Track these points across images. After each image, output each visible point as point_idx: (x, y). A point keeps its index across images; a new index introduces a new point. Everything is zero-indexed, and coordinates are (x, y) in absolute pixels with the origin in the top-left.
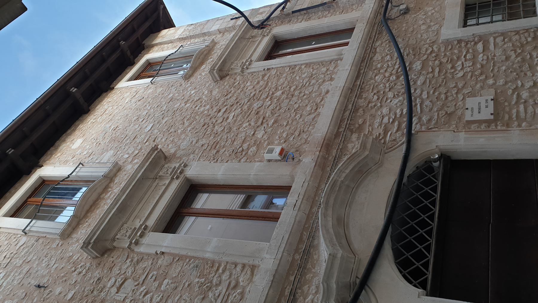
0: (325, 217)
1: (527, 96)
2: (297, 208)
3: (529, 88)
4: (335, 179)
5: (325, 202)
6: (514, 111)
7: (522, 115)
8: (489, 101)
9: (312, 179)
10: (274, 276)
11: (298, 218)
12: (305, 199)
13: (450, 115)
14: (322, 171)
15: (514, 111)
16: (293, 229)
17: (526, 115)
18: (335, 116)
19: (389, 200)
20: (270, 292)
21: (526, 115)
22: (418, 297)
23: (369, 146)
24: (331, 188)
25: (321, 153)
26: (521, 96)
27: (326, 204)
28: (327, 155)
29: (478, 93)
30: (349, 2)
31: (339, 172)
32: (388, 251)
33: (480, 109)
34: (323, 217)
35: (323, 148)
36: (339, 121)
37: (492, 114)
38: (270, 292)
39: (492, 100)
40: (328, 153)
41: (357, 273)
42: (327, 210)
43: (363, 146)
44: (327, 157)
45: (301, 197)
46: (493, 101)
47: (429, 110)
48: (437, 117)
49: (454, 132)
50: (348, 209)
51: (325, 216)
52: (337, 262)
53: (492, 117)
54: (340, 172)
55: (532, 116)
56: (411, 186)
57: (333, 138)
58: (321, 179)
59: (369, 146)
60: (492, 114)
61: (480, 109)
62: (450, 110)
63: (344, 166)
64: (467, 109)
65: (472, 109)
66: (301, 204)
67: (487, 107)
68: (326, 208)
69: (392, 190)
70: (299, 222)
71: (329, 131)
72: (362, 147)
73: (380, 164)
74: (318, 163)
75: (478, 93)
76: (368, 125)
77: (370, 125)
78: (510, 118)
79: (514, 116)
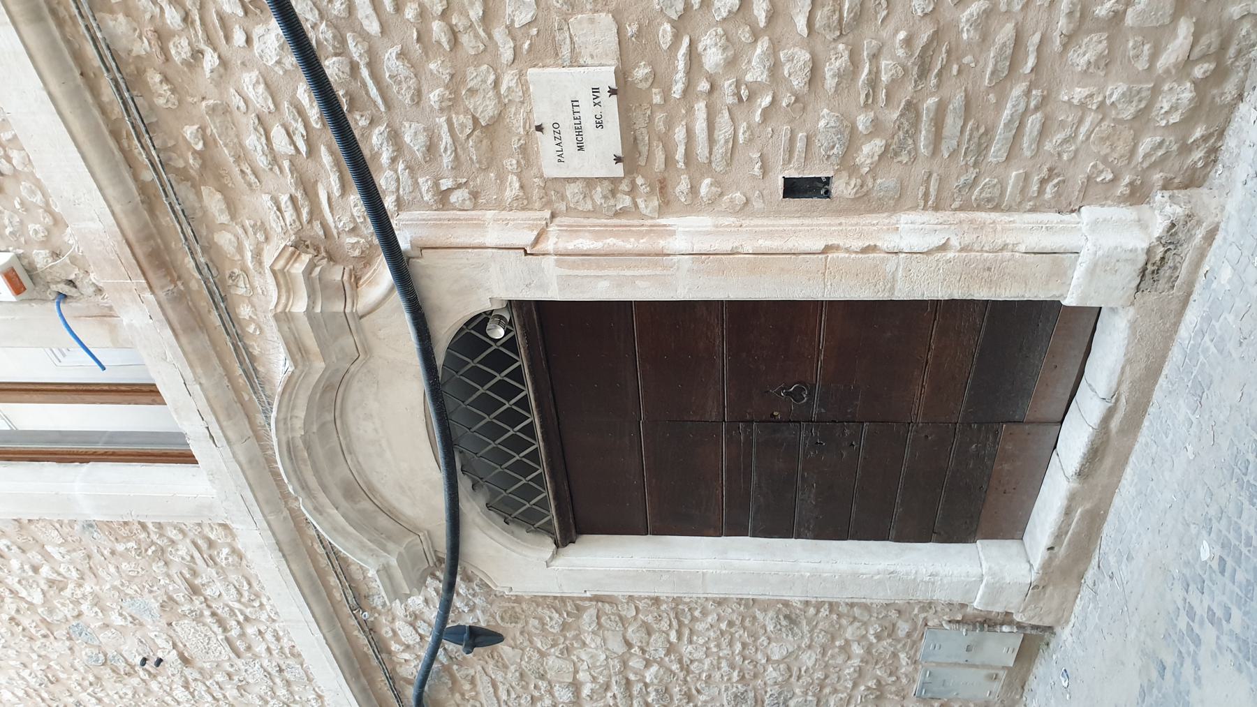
0: (321, 514)
1: (717, 65)
2: (221, 441)
3: (724, 19)
4: (284, 439)
5: (299, 489)
6: (680, 134)
7: (701, 150)
8: (604, 94)
9: (199, 371)
10: (281, 550)
11: (242, 459)
12: (222, 418)
13: (490, 130)
14: (203, 332)
15: (680, 134)
16: (254, 486)
17: (711, 154)
18: (81, 137)
19: (432, 435)
20: (294, 567)
21: (711, 154)
22: (547, 567)
23: (311, 342)
24: (291, 459)
25: (162, 294)
26: (700, 55)
27: (303, 489)
28: (179, 283)
29: (560, 29)
30: (86, 683)
31: (281, 425)
32: (472, 509)
33: (579, 131)
34: (318, 516)
35: (150, 274)
36: (112, 143)
37: (618, 160)
38: (294, 567)
39: (612, 92)
40: (175, 275)
41: (432, 547)
42: (314, 497)
43: (297, 350)
44: (182, 288)
45: (210, 418)
46: (614, 97)
47: (412, 100)
48: (450, 141)
49: (526, 254)
50: (352, 460)
51: (318, 510)
52: (398, 574)
53: (619, 170)
54: (285, 423)
55: (726, 153)
56: (470, 400)
57: (148, 217)
58: (218, 349)
59: (311, 342)
60: (618, 160)
61: (579, 131)
62: (486, 107)
63: (284, 409)
64: (539, 128)
65: (556, 125)
66: (223, 431)
67: (600, 124)
68: (310, 494)
69: (428, 418)
70: (250, 462)
71: (117, 208)
72: (298, 357)
73: (364, 351)
74: (177, 326)
75: (560, 29)
76: (231, 160)
77: (238, 159)
78: (669, 160)
79: (680, 155)
